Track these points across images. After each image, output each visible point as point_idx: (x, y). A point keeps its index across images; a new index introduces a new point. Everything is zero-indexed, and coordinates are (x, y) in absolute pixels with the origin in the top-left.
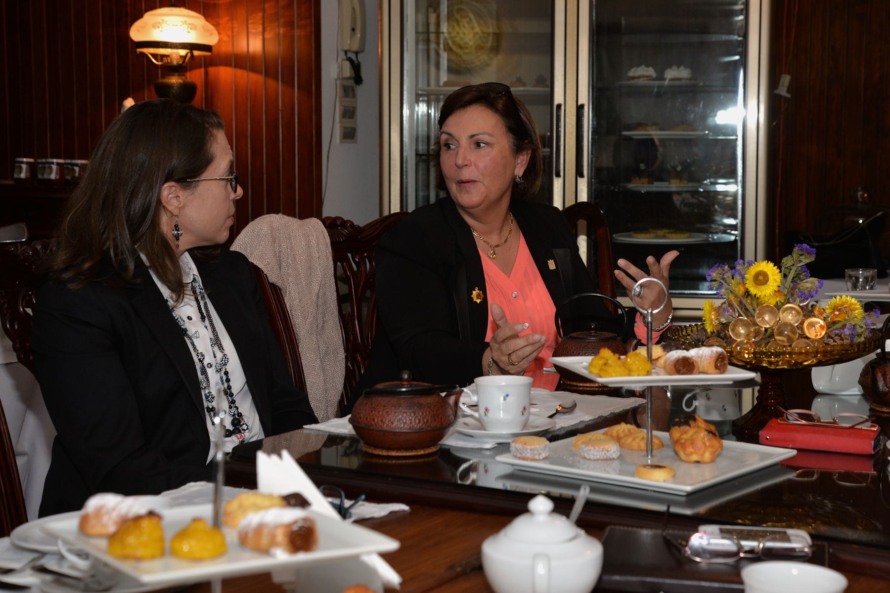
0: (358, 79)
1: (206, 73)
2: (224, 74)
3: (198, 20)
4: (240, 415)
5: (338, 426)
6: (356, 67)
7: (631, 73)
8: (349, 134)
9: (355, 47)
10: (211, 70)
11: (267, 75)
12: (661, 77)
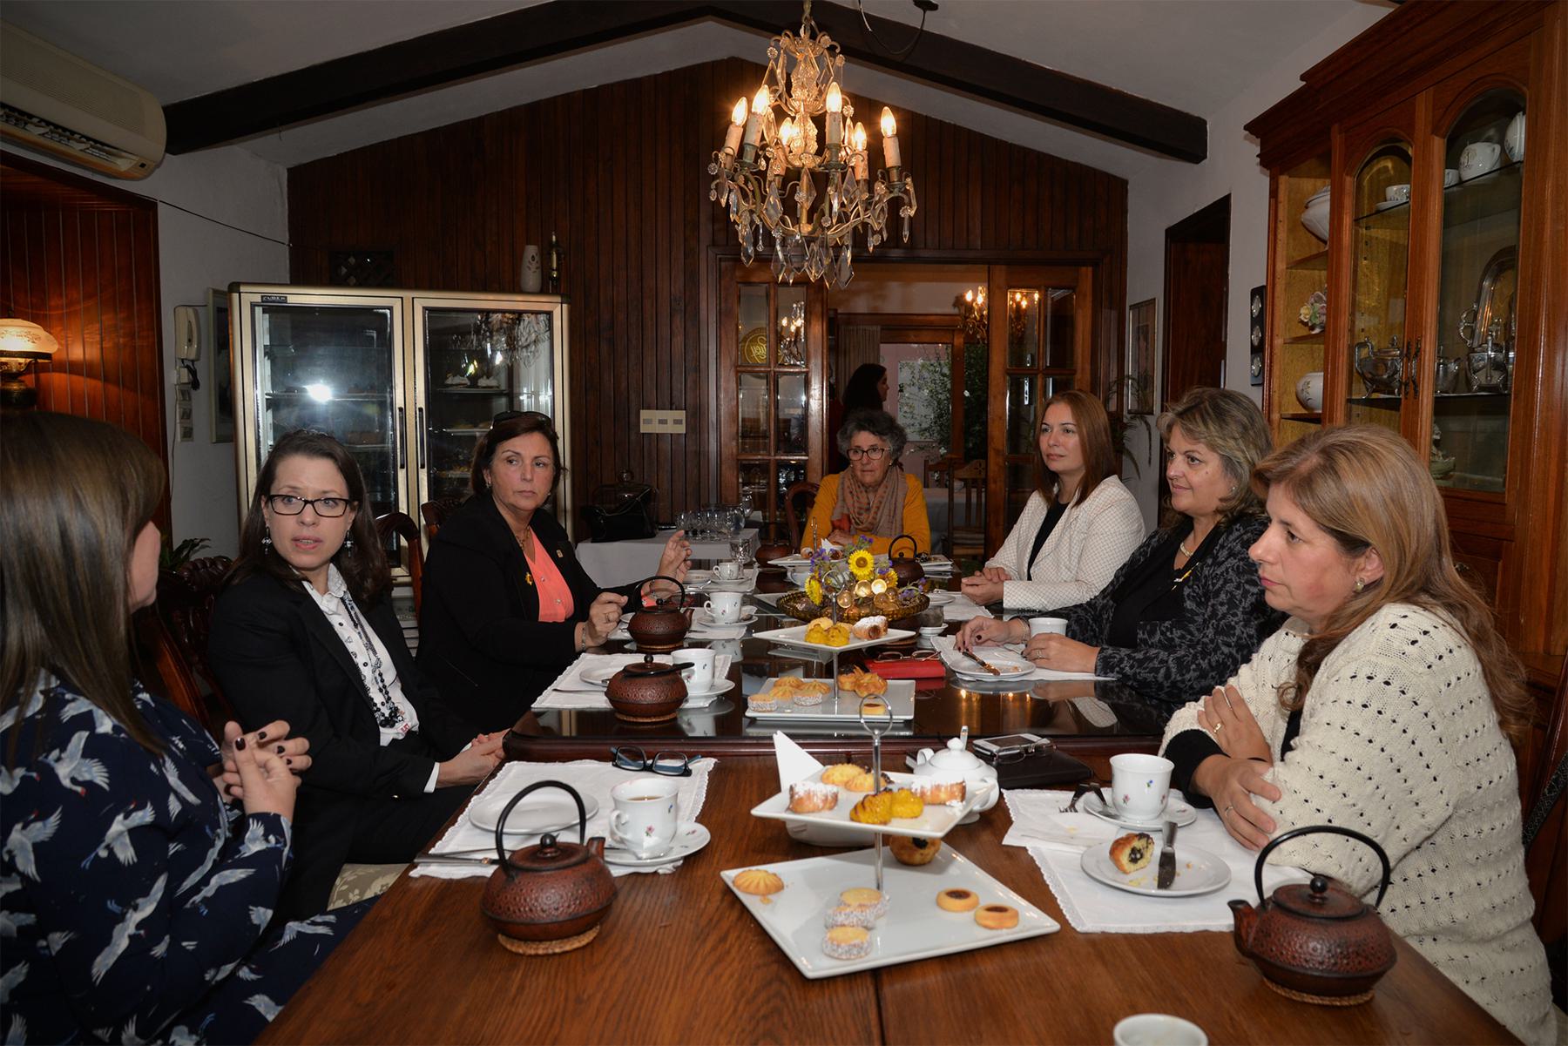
0: (195, 384)
1: (37, 379)
2: (58, 380)
3: (39, 331)
4: (396, 709)
5: (608, 665)
6: (193, 372)
7: (449, 381)
8: (188, 434)
9: (193, 356)
10: (42, 375)
11: (106, 380)
12: (542, 425)
